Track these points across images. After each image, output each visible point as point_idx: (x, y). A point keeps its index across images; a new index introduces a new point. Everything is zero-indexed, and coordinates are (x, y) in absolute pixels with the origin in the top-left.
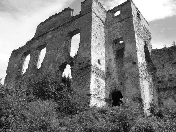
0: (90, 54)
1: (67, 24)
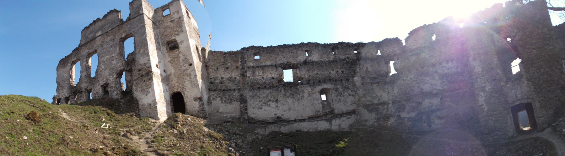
0: (149, 60)
1: (117, 28)
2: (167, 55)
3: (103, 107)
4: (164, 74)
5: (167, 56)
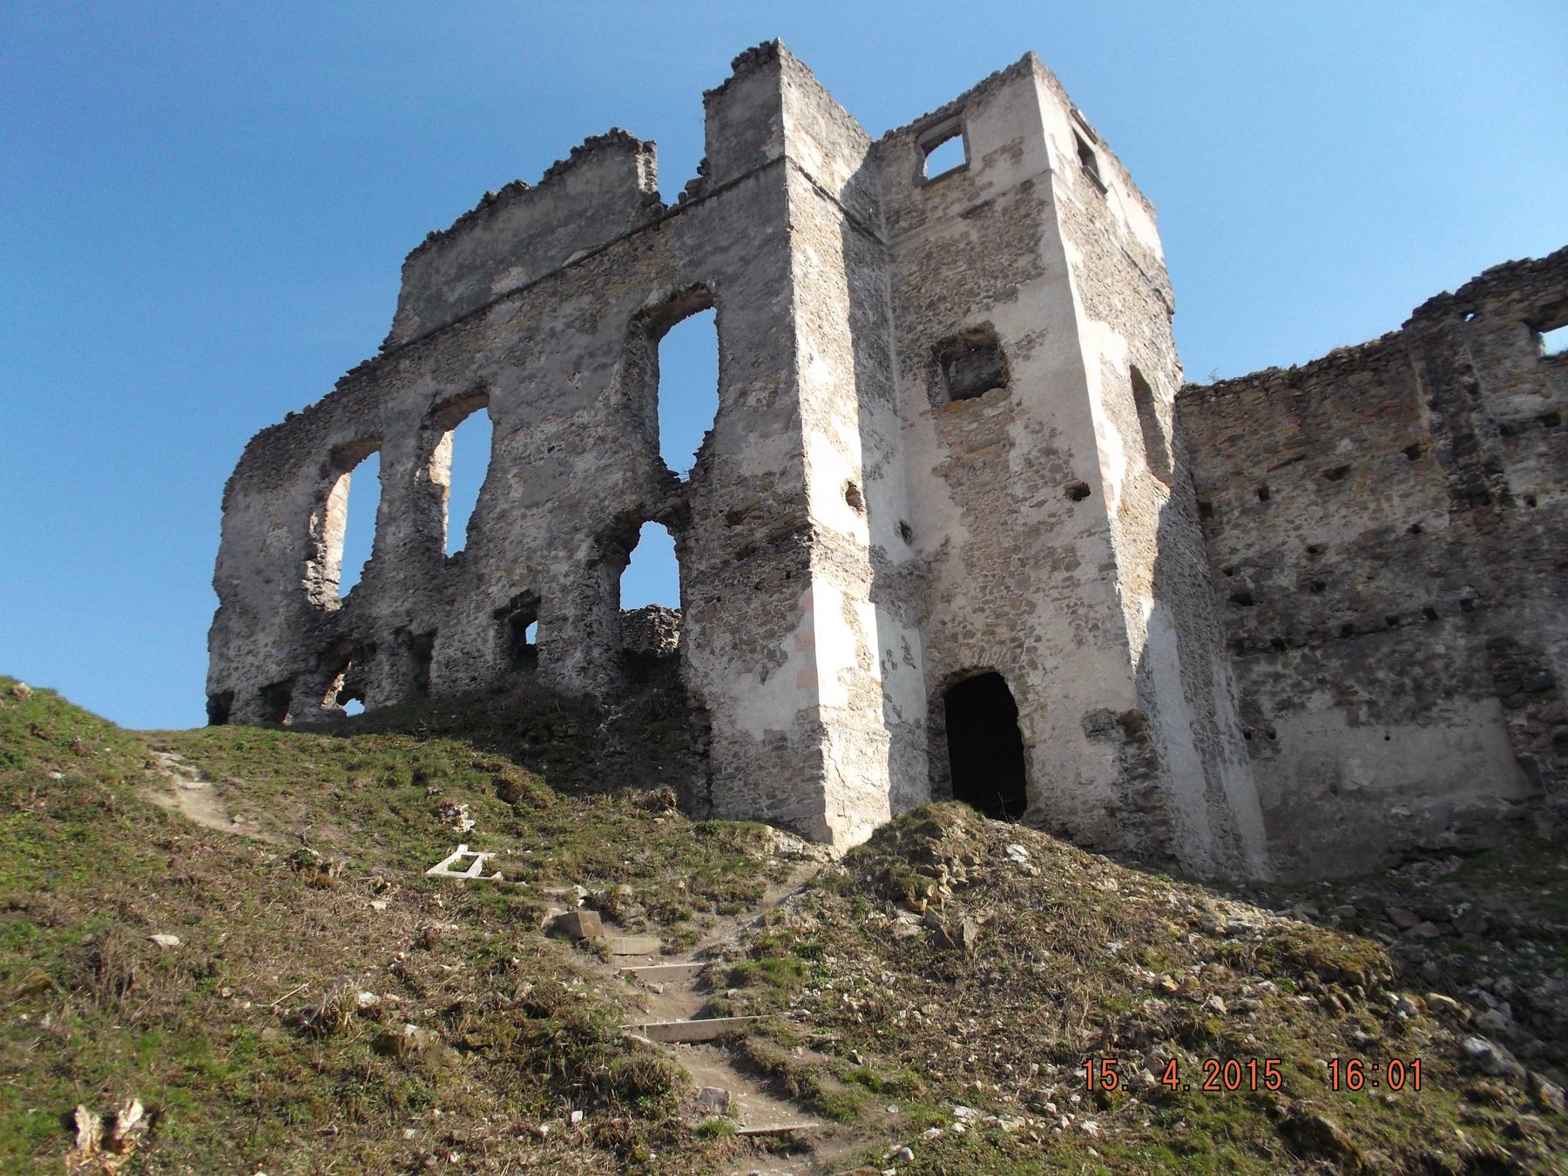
2: (928, 428)
3: (478, 746)
4: (899, 553)
5: (931, 435)
